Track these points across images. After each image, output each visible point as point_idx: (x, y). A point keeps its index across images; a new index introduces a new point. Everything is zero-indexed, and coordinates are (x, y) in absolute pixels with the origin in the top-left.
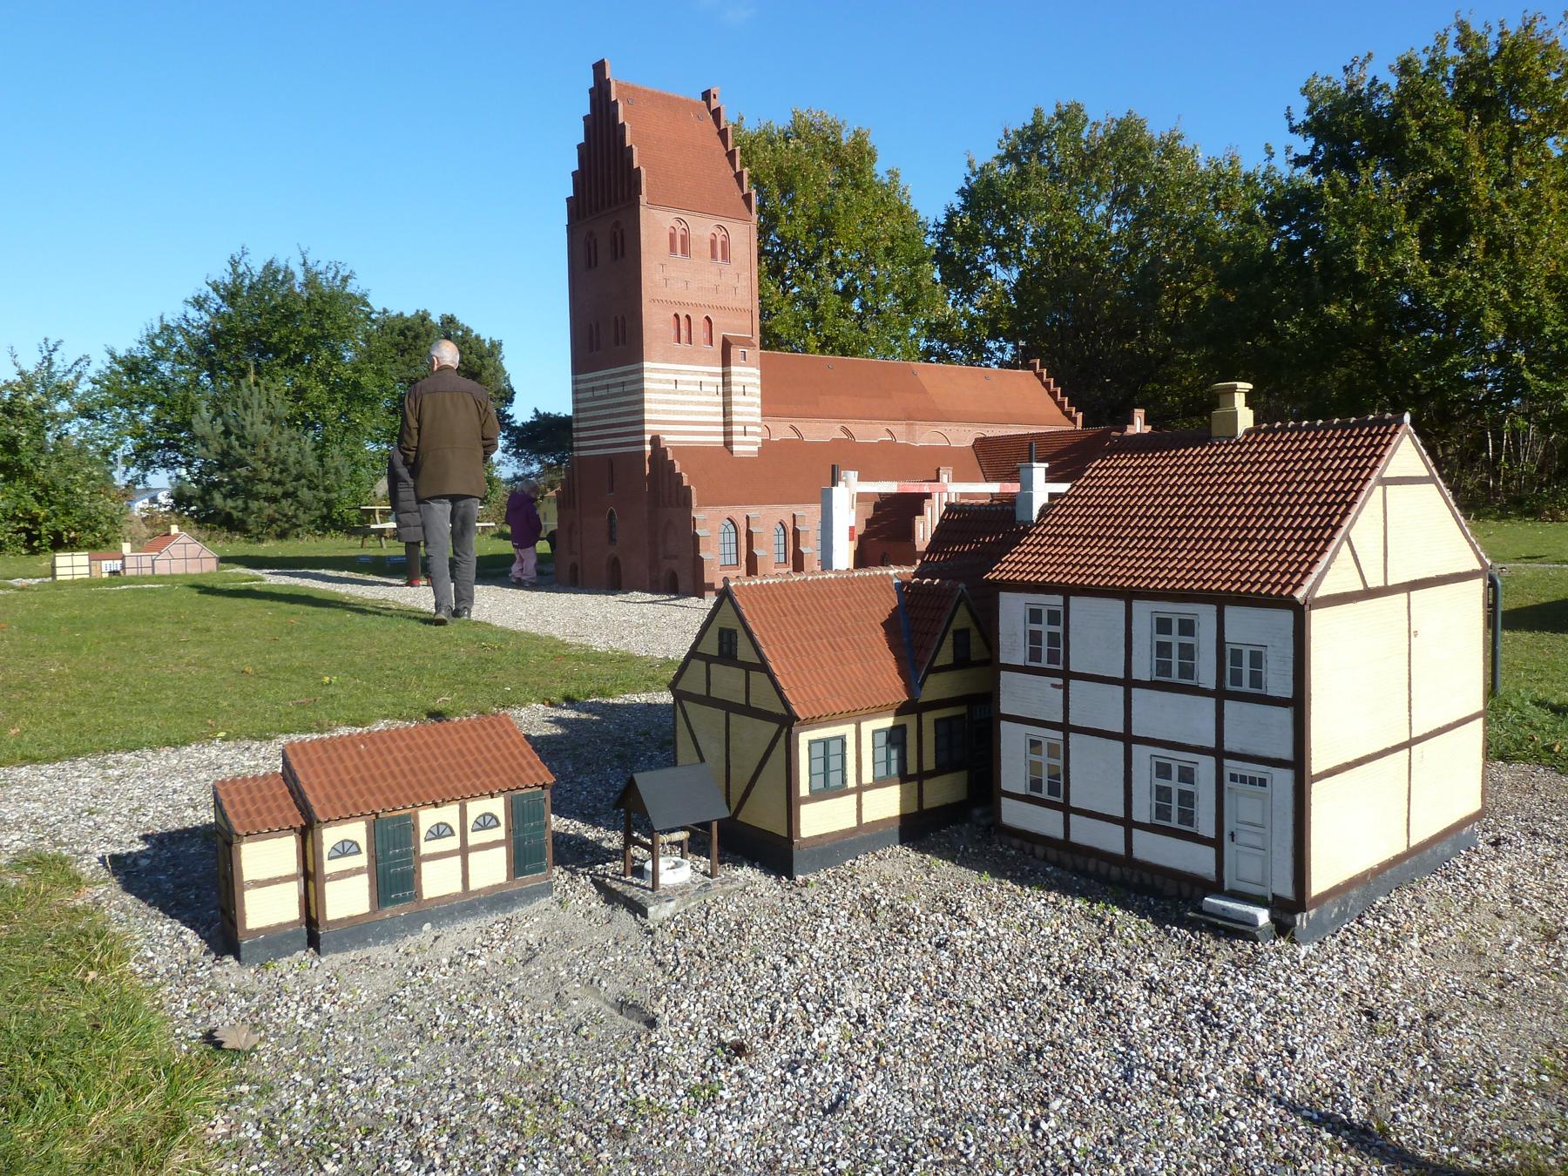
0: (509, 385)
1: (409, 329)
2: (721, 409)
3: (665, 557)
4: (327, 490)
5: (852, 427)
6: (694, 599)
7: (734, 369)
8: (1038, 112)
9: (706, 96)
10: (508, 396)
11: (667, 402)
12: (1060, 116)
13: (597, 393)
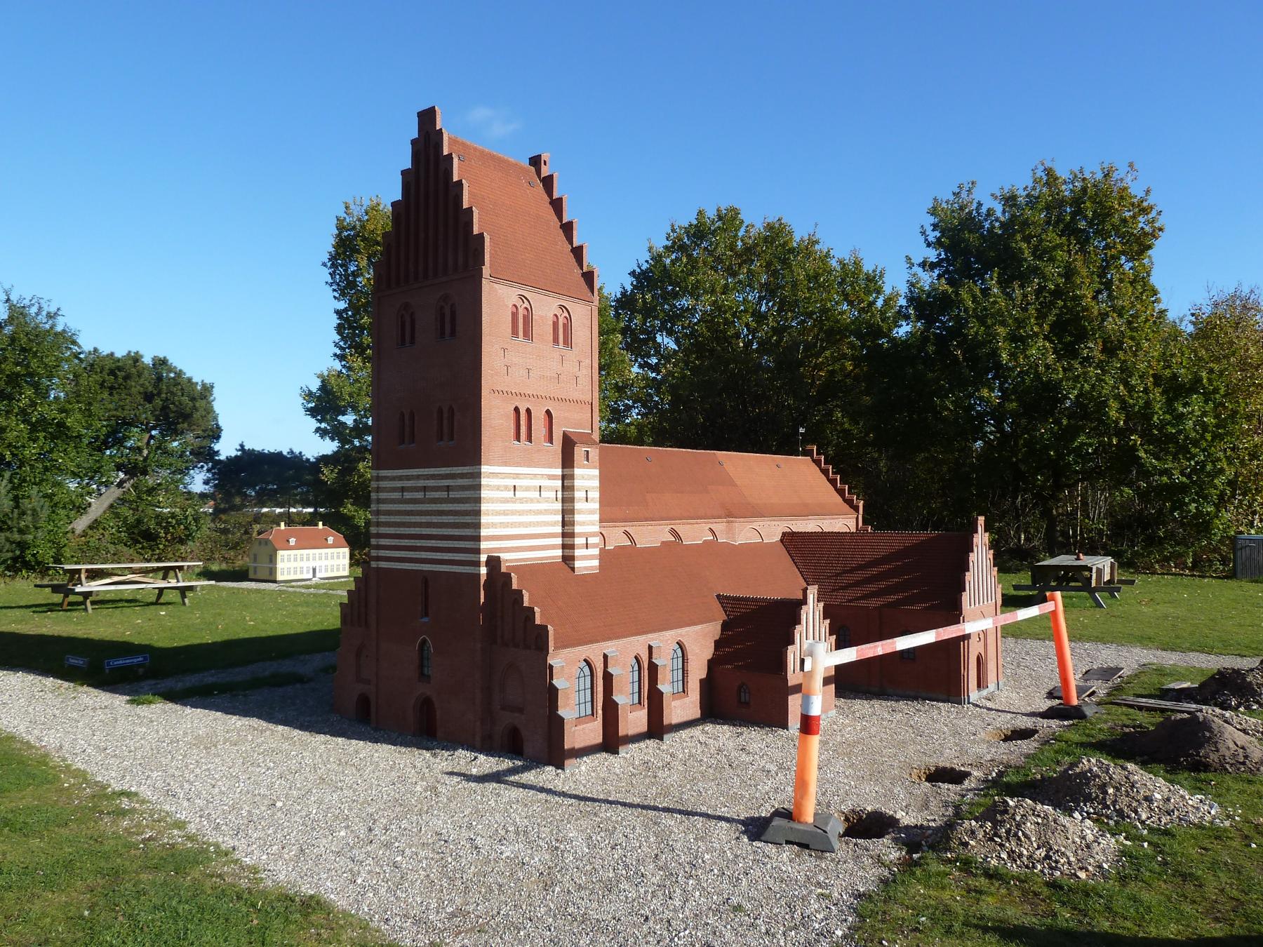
0: (217, 425)
1: (120, 369)
2: (559, 518)
3: (503, 709)
4: (21, 531)
5: (681, 529)
6: (550, 769)
7: (577, 471)
8: (700, 213)
9: (536, 161)
10: (216, 434)
11: (505, 513)
12: (720, 218)
13: (408, 495)
